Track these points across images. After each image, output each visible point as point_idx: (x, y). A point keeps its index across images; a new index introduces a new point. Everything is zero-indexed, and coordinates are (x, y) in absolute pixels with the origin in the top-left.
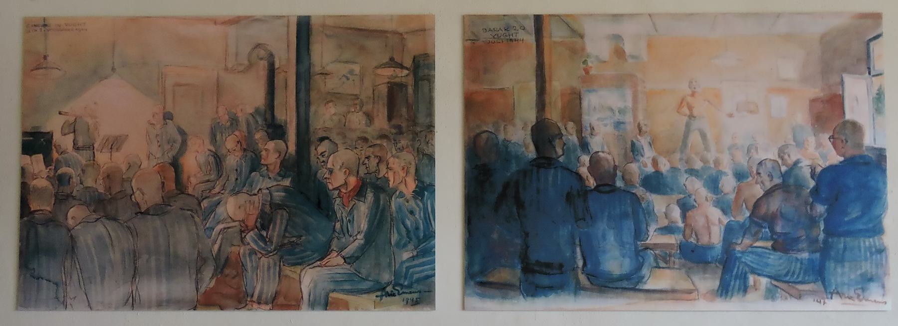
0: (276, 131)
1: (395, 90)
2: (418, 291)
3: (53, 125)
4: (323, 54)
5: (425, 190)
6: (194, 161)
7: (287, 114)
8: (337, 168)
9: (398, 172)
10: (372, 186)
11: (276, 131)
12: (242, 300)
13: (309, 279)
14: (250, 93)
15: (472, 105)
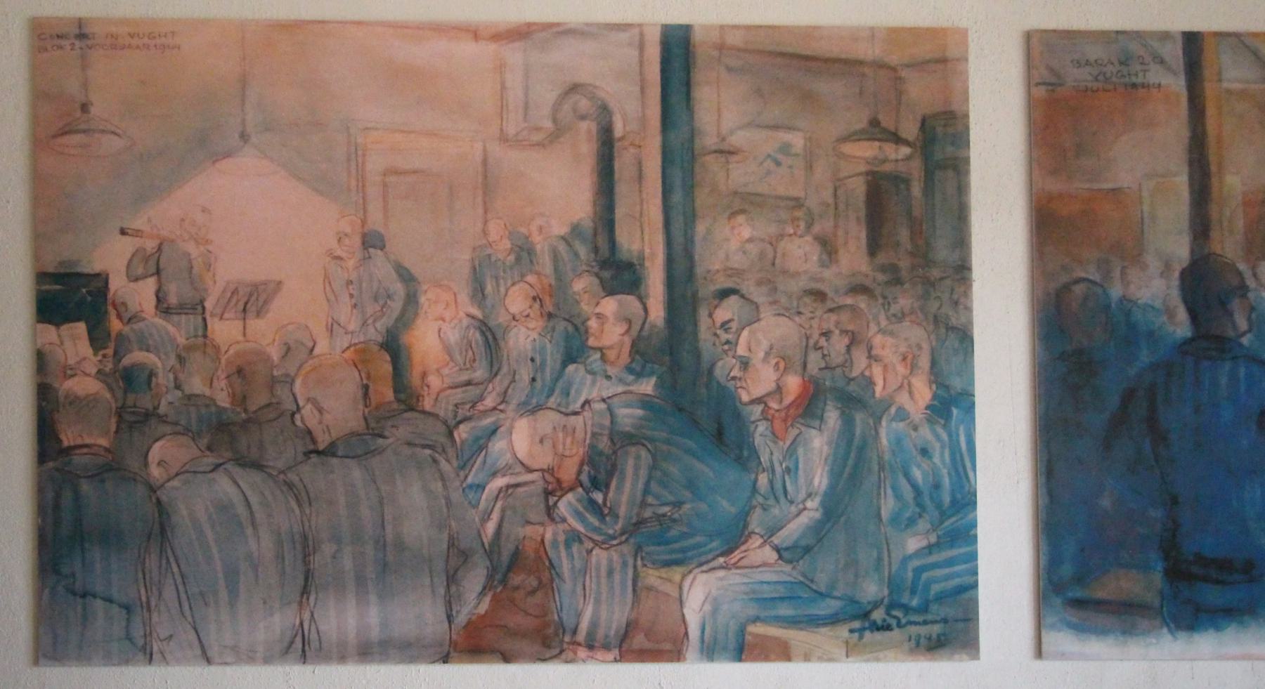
0: (620, 275)
1: (881, 194)
2: (945, 624)
3: (110, 257)
4: (721, 109)
5: (953, 403)
6: (436, 338)
7: (643, 237)
8: (757, 355)
9: (892, 362)
10: (830, 393)
11: (620, 275)
12: (550, 640)
13: (700, 595)
14: (559, 192)
15: (1050, 224)
